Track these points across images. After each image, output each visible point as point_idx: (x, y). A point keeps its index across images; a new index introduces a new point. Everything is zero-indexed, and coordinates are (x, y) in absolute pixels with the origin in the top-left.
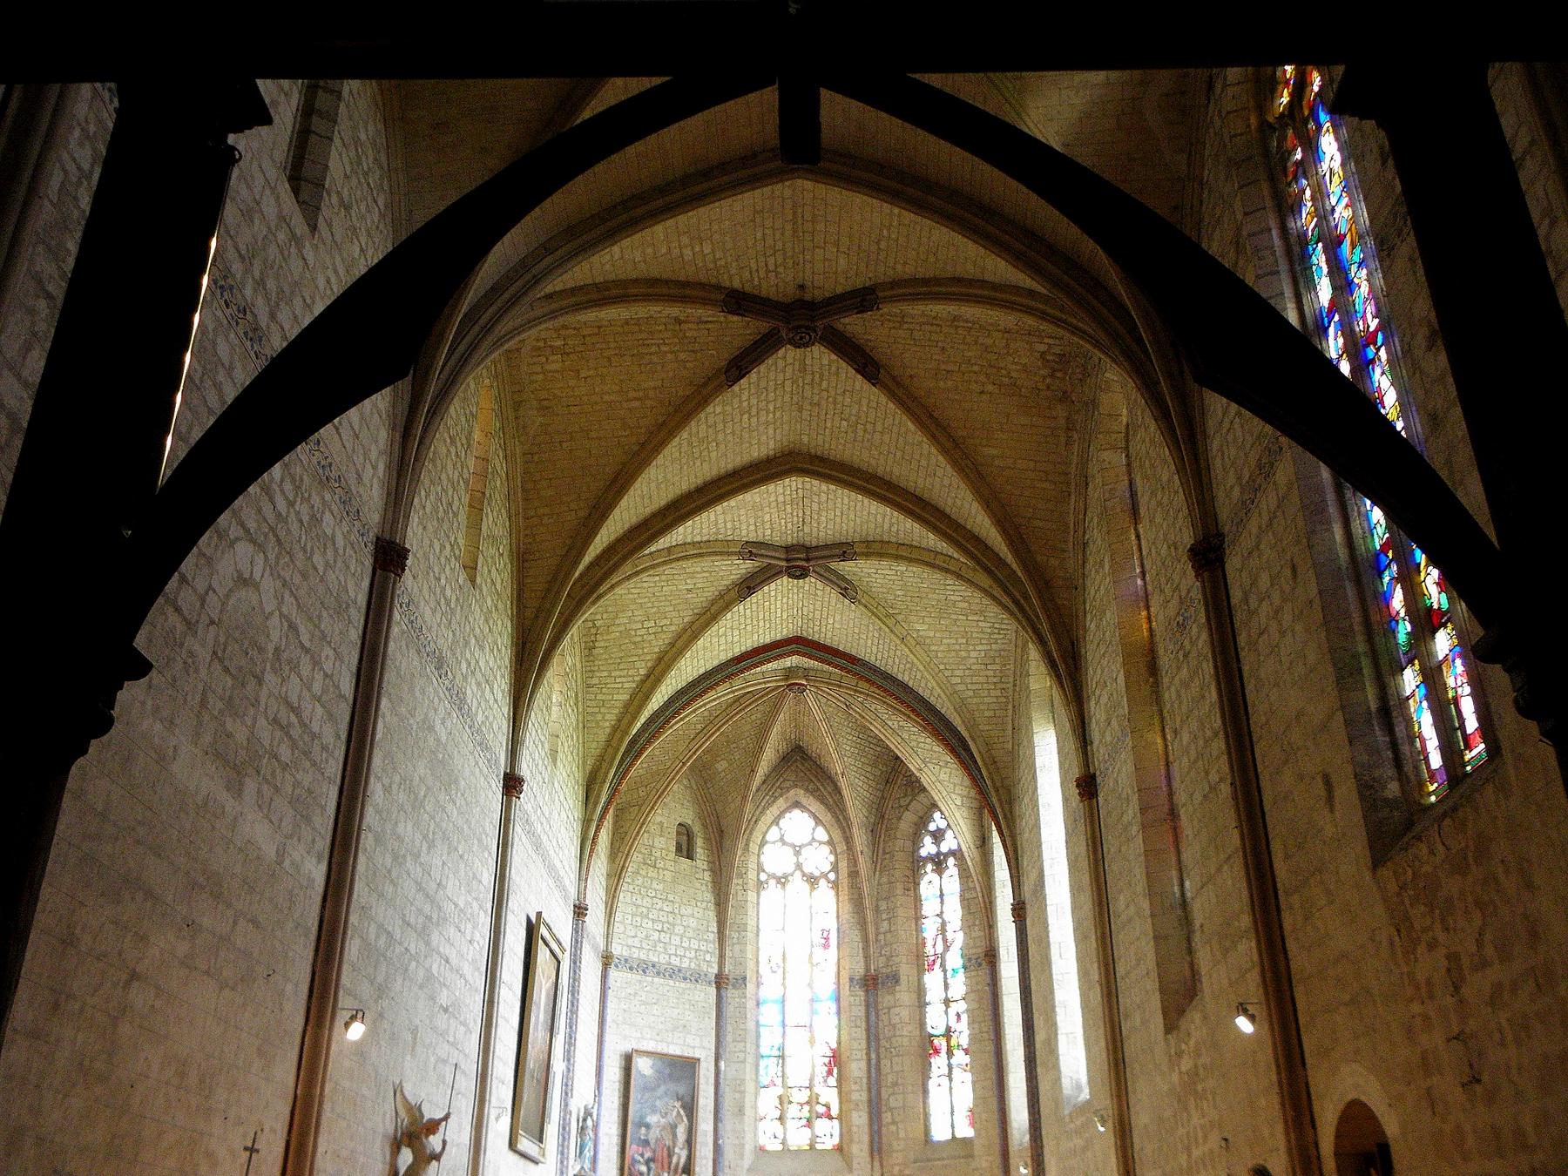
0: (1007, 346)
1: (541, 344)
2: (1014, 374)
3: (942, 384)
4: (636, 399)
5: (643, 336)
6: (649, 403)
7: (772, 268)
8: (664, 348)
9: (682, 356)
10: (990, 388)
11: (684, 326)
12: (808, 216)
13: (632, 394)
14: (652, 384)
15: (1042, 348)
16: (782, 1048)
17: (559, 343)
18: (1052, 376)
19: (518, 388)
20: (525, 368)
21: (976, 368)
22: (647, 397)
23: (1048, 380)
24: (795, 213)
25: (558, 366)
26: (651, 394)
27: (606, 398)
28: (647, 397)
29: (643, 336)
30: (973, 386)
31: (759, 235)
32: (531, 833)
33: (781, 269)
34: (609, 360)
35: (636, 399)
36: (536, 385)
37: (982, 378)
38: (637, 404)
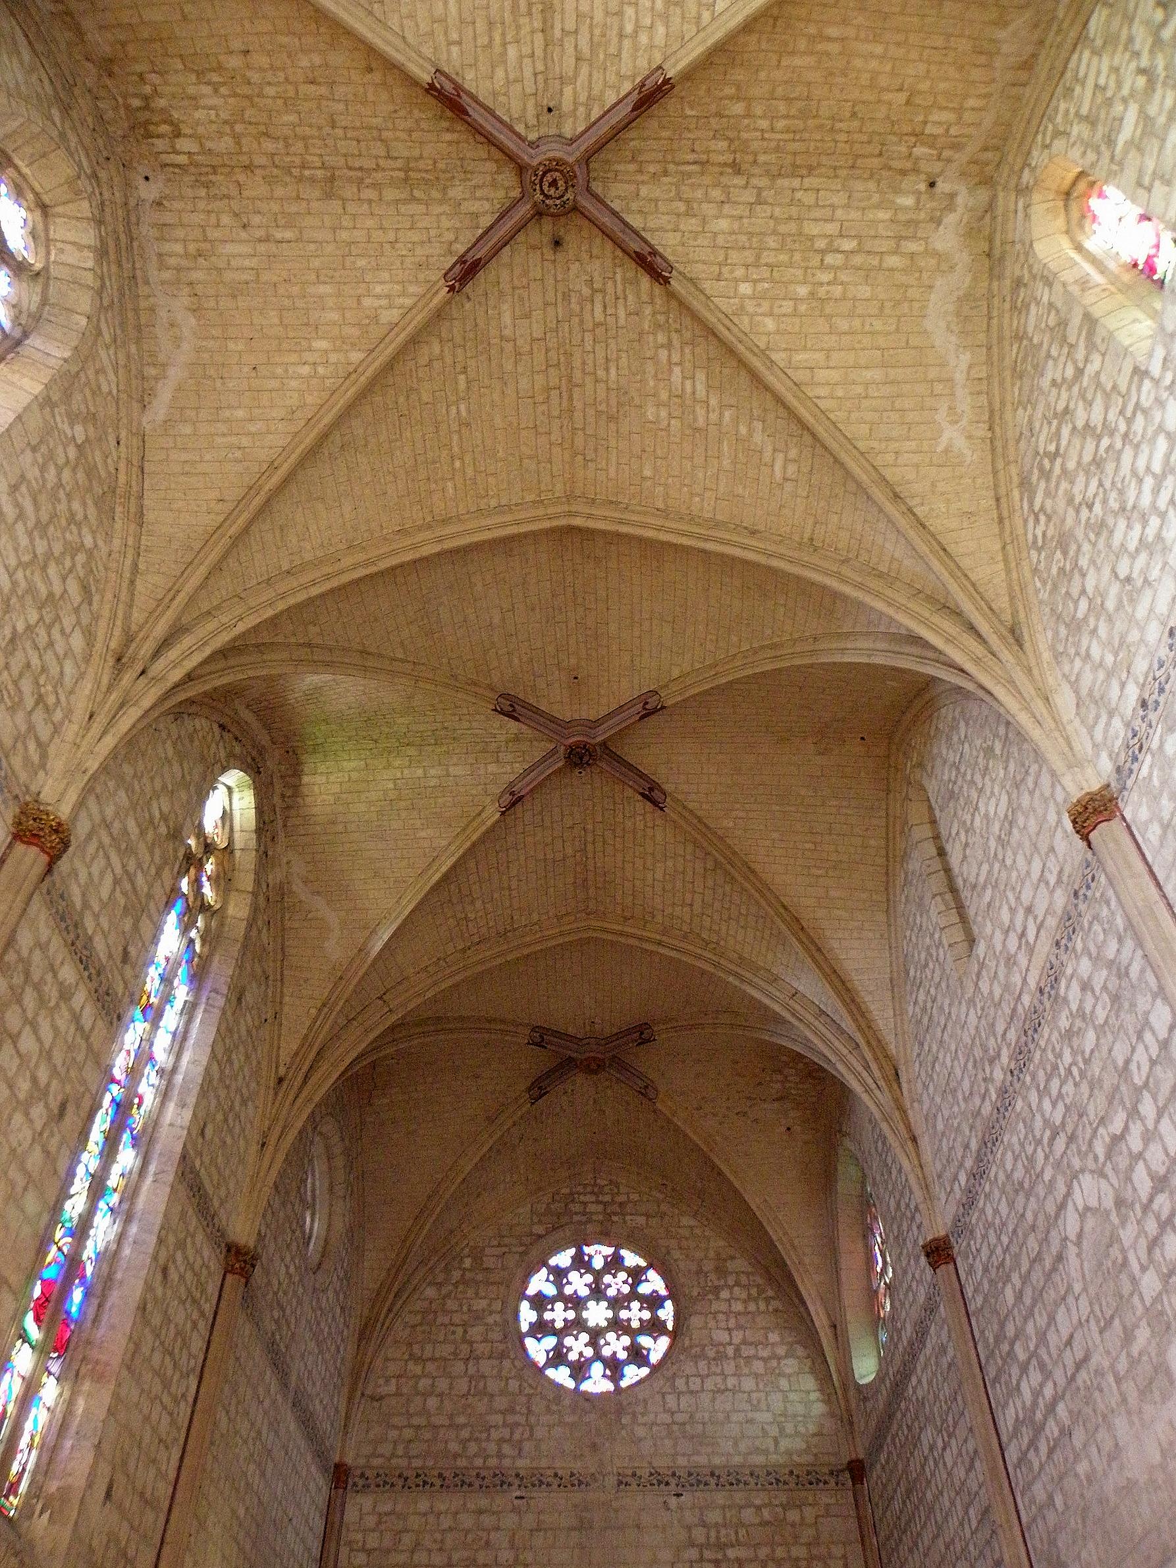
0: (237, 138)
1: (946, 153)
2: (206, 90)
3: (317, 60)
4: (829, 39)
5: (793, 146)
6: (812, 30)
7: (598, 298)
8: (764, 124)
9: (738, 108)
10: (234, 62)
11: (727, 157)
12: (555, 400)
13: (834, 48)
14: (798, 61)
15: (184, 144)
16: (521, 798)
17: (919, 151)
18: (146, 98)
19: (1015, 91)
20: (988, 119)
21: (270, 91)
22: (812, 39)
23: (148, 89)
24: (571, 398)
25: (936, 116)
26: (802, 45)
27: (879, 49)
28: (812, 39)
29: (793, 146)
30: (264, 61)
31: (613, 371)
32: (1167, 1154)
33: (586, 291)
34: (854, 115)
35: (829, 39)
36: (983, 90)
37: (255, 77)
38: (833, 31)
